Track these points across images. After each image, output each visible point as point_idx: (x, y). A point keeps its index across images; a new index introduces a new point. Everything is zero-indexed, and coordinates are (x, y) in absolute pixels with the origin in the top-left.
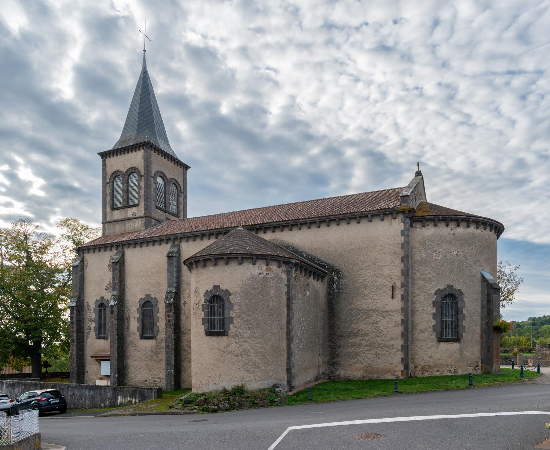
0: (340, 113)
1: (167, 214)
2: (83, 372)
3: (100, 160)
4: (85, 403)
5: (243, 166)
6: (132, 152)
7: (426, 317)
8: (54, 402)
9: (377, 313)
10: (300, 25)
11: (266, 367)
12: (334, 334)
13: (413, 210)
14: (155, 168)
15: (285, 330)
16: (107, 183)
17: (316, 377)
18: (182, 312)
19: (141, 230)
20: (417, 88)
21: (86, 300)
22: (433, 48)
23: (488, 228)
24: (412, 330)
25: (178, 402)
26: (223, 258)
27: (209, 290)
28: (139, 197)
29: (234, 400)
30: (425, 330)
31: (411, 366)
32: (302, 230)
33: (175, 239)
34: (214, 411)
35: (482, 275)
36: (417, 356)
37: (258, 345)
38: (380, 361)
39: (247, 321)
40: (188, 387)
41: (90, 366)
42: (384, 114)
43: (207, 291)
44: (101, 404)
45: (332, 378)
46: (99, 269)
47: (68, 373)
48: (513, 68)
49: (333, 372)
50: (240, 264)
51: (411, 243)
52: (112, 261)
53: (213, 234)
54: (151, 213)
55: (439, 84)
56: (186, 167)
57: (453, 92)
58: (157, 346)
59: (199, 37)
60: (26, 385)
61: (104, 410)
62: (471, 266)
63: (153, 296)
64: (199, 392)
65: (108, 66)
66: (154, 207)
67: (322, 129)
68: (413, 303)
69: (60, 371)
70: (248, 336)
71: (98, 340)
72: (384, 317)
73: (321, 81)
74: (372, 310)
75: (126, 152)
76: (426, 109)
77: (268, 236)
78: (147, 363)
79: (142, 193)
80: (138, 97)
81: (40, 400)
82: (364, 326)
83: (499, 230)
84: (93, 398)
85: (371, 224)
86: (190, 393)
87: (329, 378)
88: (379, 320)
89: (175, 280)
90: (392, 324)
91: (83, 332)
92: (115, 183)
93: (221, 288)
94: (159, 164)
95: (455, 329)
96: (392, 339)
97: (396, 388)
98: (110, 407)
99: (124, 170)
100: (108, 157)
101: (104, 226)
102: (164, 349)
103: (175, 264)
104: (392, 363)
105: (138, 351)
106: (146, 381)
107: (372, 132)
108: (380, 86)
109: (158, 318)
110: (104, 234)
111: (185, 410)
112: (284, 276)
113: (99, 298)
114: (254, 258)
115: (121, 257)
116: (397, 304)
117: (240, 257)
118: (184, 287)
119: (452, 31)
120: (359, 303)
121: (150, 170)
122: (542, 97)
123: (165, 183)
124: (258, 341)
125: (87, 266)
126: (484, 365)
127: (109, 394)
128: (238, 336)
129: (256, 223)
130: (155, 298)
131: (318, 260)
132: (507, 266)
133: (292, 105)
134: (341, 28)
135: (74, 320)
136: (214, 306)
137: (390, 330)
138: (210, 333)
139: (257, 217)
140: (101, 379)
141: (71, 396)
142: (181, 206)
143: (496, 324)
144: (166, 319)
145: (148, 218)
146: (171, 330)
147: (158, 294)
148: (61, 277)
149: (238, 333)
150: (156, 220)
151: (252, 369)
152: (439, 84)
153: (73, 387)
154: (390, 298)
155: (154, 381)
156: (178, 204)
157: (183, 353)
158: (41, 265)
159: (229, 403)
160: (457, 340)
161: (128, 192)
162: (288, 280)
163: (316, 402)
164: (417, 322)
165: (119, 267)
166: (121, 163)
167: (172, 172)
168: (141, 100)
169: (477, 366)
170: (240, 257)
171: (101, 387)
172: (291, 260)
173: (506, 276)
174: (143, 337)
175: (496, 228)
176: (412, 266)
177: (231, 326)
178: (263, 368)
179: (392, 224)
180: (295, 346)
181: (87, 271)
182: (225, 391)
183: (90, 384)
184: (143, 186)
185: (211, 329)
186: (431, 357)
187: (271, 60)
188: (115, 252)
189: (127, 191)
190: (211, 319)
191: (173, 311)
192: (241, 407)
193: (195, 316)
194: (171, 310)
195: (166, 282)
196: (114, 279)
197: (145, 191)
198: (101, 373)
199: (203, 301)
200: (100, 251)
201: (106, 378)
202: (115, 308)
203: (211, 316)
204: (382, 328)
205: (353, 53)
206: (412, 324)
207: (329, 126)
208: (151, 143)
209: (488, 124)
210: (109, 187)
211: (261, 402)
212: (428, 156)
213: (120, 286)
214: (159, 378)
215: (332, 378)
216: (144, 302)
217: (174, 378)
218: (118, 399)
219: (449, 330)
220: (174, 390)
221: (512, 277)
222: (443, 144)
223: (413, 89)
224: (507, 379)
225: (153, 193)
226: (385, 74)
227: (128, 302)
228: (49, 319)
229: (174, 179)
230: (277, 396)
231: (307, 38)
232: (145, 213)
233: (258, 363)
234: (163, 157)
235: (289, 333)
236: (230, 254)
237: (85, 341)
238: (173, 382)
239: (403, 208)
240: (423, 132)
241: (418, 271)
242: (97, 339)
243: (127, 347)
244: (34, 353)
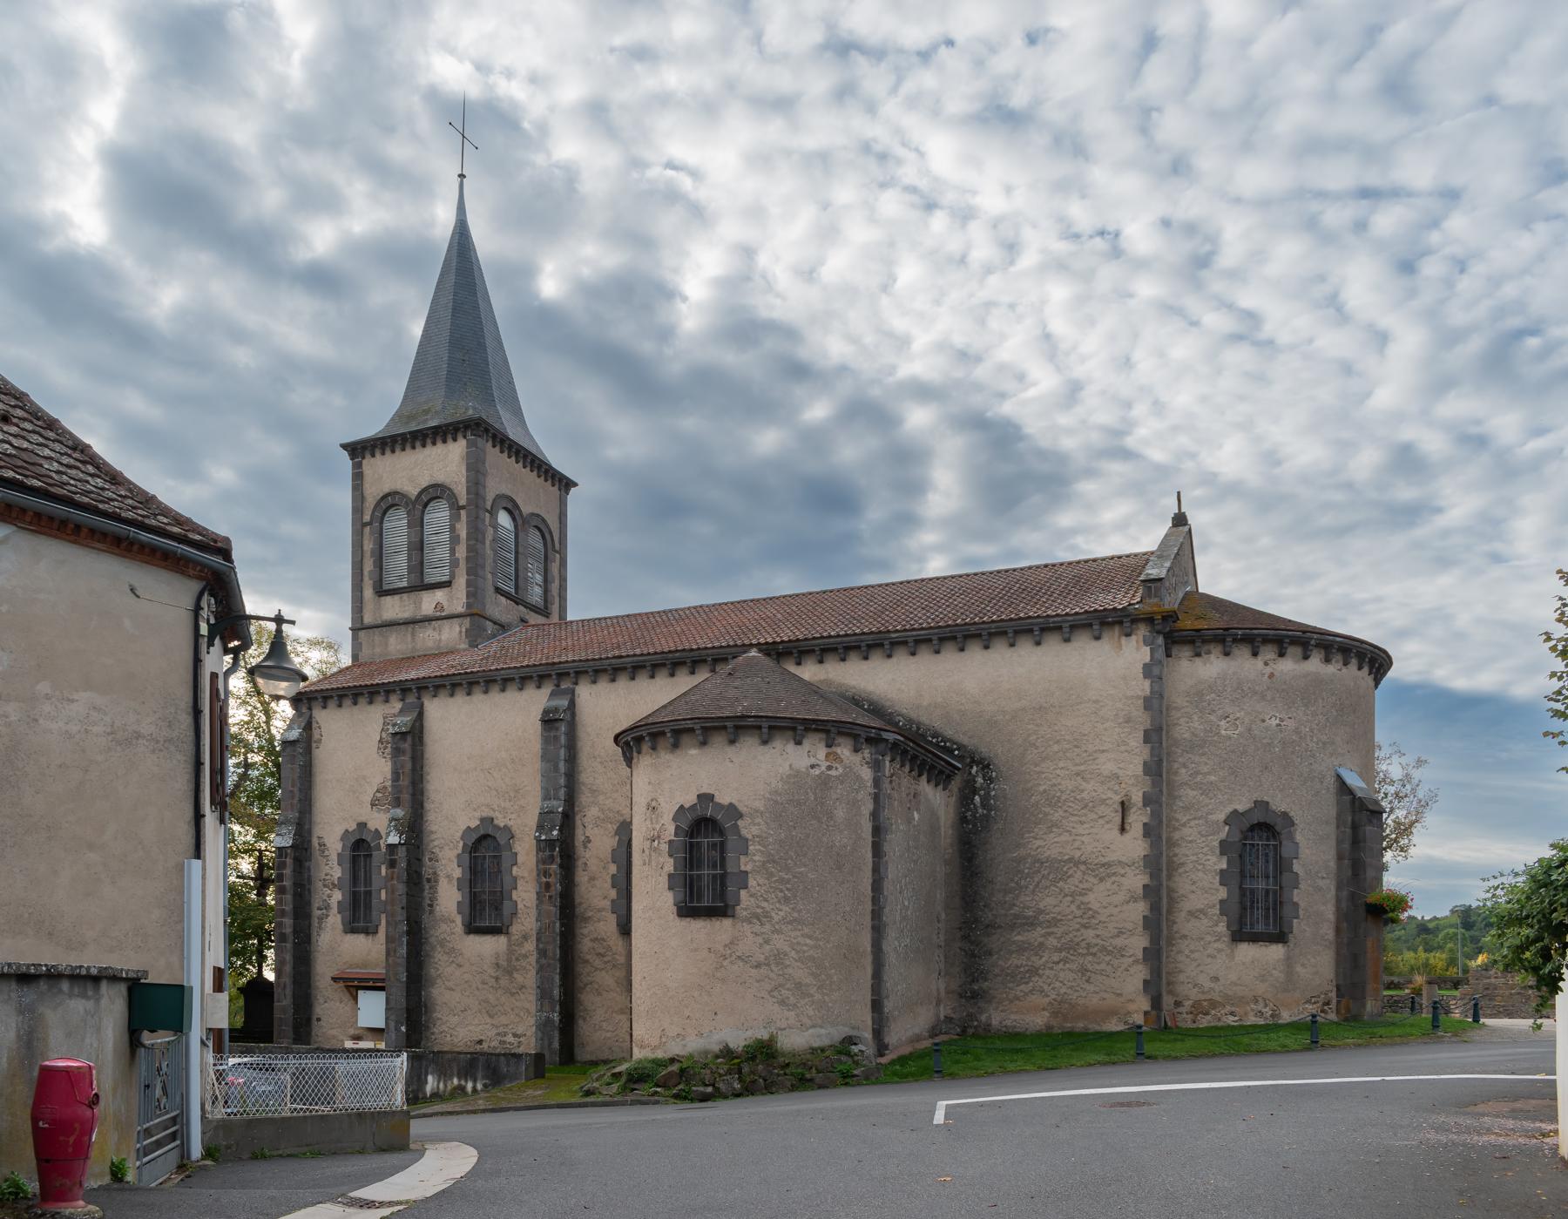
0: (885, 301)
2: (309, 1020)
5: (613, 453)
7: (1203, 881)
9: (1083, 867)
10: (758, 39)
12: (976, 920)
13: (1169, 614)
14: (495, 487)
15: (869, 907)
16: (364, 525)
17: (933, 1028)
18: (580, 863)
19: (458, 651)
20: (1102, 233)
21: (318, 831)
22: (1144, 117)
23: (1354, 661)
24: (1169, 912)
28: (454, 563)
29: (752, 1072)
30: (1201, 911)
31: (1167, 1001)
32: (894, 660)
33: (562, 675)
34: (705, 1098)
35: (1339, 777)
36: (1182, 977)
38: (1091, 988)
39: (781, 881)
42: (1012, 306)
45: (971, 1031)
48: (1372, 178)
49: (971, 1016)
51: (1166, 695)
53: (664, 665)
55: (1166, 223)
57: (1208, 247)
58: (510, 952)
59: (468, 67)
62: (1313, 756)
63: (500, 822)
65: (202, 148)
66: (492, 589)
67: (833, 348)
68: (1172, 844)
71: (350, 938)
72: (1101, 880)
73: (825, 206)
74: (1071, 860)
75: (418, 444)
76: (1131, 296)
77: (809, 672)
78: (485, 992)
79: (461, 552)
82: (1050, 901)
83: (1381, 665)
85: (1068, 647)
87: (964, 1031)
88: (1085, 886)
89: (562, 781)
90: (1121, 897)
91: (308, 916)
93: (717, 799)
94: (503, 476)
95: (1275, 909)
96: (1120, 933)
97: (1139, 1046)
99: (413, 491)
100: (368, 456)
103: (563, 740)
104: (1122, 992)
106: (480, 1042)
107: (978, 359)
108: (996, 224)
109: (515, 879)
110: (355, 657)
112: (867, 774)
113: (352, 826)
114: (798, 729)
116: (1133, 846)
117: (765, 725)
119: (1195, 70)
120: (1038, 843)
122: (1461, 266)
123: (516, 527)
124: (806, 930)
126: (1344, 1001)
128: (758, 917)
130: (507, 828)
131: (935, 735)
132: (1395, 759)
133: (742, 277)
134: (877, 54)
137: (1115, 911)
138: (688, 910)
140: (357, 1038)
142: (555, 587)
143: (1372, 898)
145: (475, 615)
146: (553, 910)
152: (1166, 223)
154: (1116, 832)
156: (546, 580)
159: (740, 1080)
160: (1280, 937)
162: (877, 783)
163: (953, 1076)
164: (1181, 892)
165: (409, 746)
166: (406, 472)
167: (533, 496)
168: (454, 309)
169: (1328, 1004)
170: (765, 725)
172: (885, 735)
173: (1392, 782)
174: (472, 929)
175: (1372, 662)
176: (1168, 754)
177: (743, 892)
178: (817, 996)
179: (1120, 647)
180: (891, 944)
181: (321, 755)
182: (727, 1053)
184: (463, 534)
185: (691, 901)
186: (1216, 979)
187: (678, 143)
188: (399, 705)
189: (418, 547)
193: (646, 868)
196: (396, 775)
197: (470, 549)
199: (670, 831)
200: (355, 703)
204: (1095, 906)
205: (913, 123)
206: (1169, 896)
207: (854, 340)
209: (1310, 341)
210: (371, 533)
211: (819, 1078)
212: (1142, 432)
213: (413, 795)
214: (515, 1035)
215: (971, 1031)
216: (475, 836)
219: (1258, 913)
221: (1408, 787)
222: (1183, 398)
223: (1091, 237)
224: (1397, 1031)
225: (489, 552)
226: (1008, 190)
227: (433, 837)
230: (857, 1063)
231: (782, 81)
232: (469, 605)
233: (807, 985)
235: (877, 914)
236: (743, 717)
237: (314, 940)
238: (556, 1045)
239: (1148, 609)
240: (1126, 363)
241: (1184, 766)
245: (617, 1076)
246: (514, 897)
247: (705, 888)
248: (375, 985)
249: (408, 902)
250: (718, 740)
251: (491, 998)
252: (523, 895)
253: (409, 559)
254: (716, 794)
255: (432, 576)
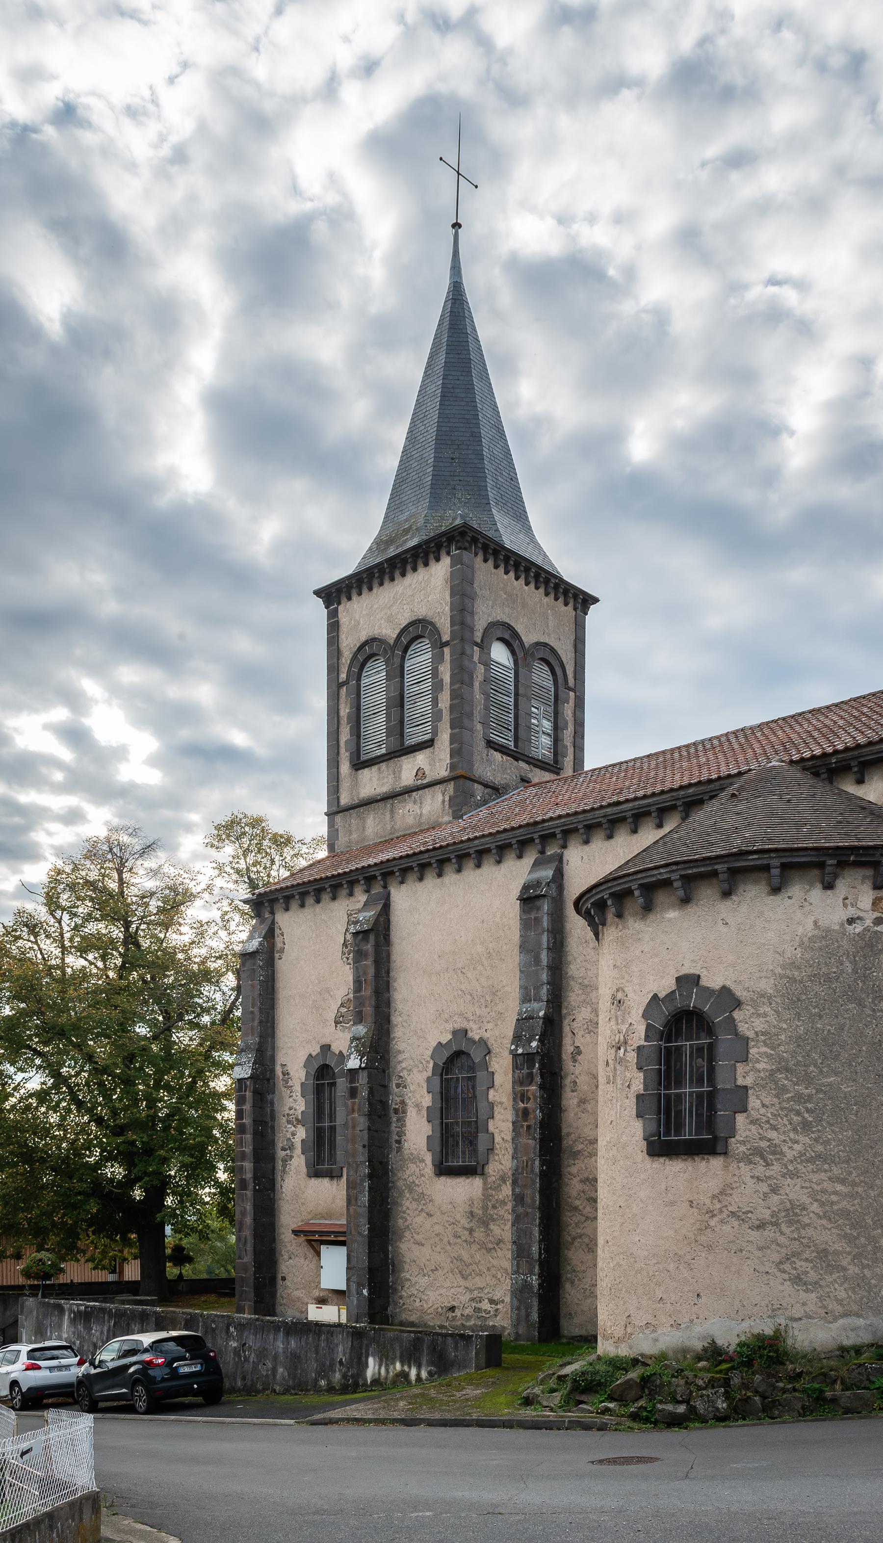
1: (522, 764)
3: (318, 610)
4: (274, 1376)
6: (415, 569)
8: (187, 1370)
11: (864, 1267)
14: (485, 613)
16: (340, 685)
18: (568, 1081)
21: (282, 1058)
25: (552, 1383)
26: (715, 874)
27: (662, 995)
28: (437, 716)
29: (745, 1386)
33: (547, 838)
34: (674, 1422)
37: (839, 1187)
39: (799, 1098)
40: (583, 1333)
41: (293, 1261)
43: (655, 996)
44: (314, 1382)
46: (317, 953)
47: (232, 1281)
50: (776, 890)
52: (352, 929)
54: (471, 764)
56: (583, 601)
58: (486, 1197)
60: (119, 1315)
61: (326, 1398)
64: (624, 1351)
66: (482, 744)
69: (224, 1276)
70: (801, 1154)
71: (315, 1182)
80: (436, 388)
81: (150, 1363)
84: (295, 1359)
86: (593, 1357)
89: (544, 977)
91: (272, 1158)
92: (364, 681)
93: (704, 982)
94: (498, 596)
98: (345, 1389)
99: (390, 633)
100: (344, 599)
101: (331, 824)
102: (509, 1206)
103: (545, 922)
105: (430, 1215)
106: (452, 1309)
109: (492, 1105)
111: (573, 1415)
113: (315, 1050)
115: (379, 915)
118: (574, 997)
121: (468, 620)
124: (836, 1171)
125: (282, 951)
127: (342, 1352)
128: (759, 1154)
129: (830, 750)
130: (483, 1042)
135: (247, 1121)
136: (678, 1048)
138: (661, 1147)
139: (831, 732)
140: (322, 1301)
141: (236, 1352)
144: (515, 1109)
145: (462, 783)
146: (532, 1144)
147: (490, 1026)
148: (218, 996)
149: (764, 1144)
150: (486, 786)
151: (813, 1276)
153: (241, 1327)
155: (477, 1310)
156: (556, 728)
157: (570, 1219)
158: (165, 960)
159: (727, 1396)
161: (402, 706)
165: (374, 946)
166: (378, 614)
168: (443, 396)
170: (775, 862)
171: (318, 1327)
174: (443, 1170)
177: (740, 1118)
178: (853, 1270)
181: (283, 966)
182: (713, 1353)
183: (290, 1315)
184: (447, 678)
185: (668, 1133)
189: (398, 703)
190: (668, 1097)
191: (538, 1079)
192: (769, 1409)
193: (610, 1087)
194: (531, 1076)
195: (517, 984)
197: (454, 695)
198: (323, 1283)
199: (639, 1037)
201: (334, 1297)
202: (363, 1079)
203: (667, 1087)
208: (472, 529)
210: (348, 695)
213: (377, 1007)
214: (492, 1301)
216: (446, 1054)
217: (540, 1303)
218: (367, 1366)
220: (539, 1341)
225: (478, 696)
227: (401, 1057)
228: (186, 1121)
229: (545, 645)
232: (453, 767)
233: (836, 1253)
234: (512, 574)
236: (742, 854)
237: (278, 1186)
238: (535, 1316)
242: (310, 1176)
243: (396, 1203)
244: (133, 1218)
245: (562, 1379)
246: (491, 1128)
247: (688, 1112)
248: (336, 1239)
249: (370, 1138)
250: (707, 893)
251: (465, 1256)
252: (500, 1124)
253: (388, 720)
254: (704, 974)
255: (414, 735)
